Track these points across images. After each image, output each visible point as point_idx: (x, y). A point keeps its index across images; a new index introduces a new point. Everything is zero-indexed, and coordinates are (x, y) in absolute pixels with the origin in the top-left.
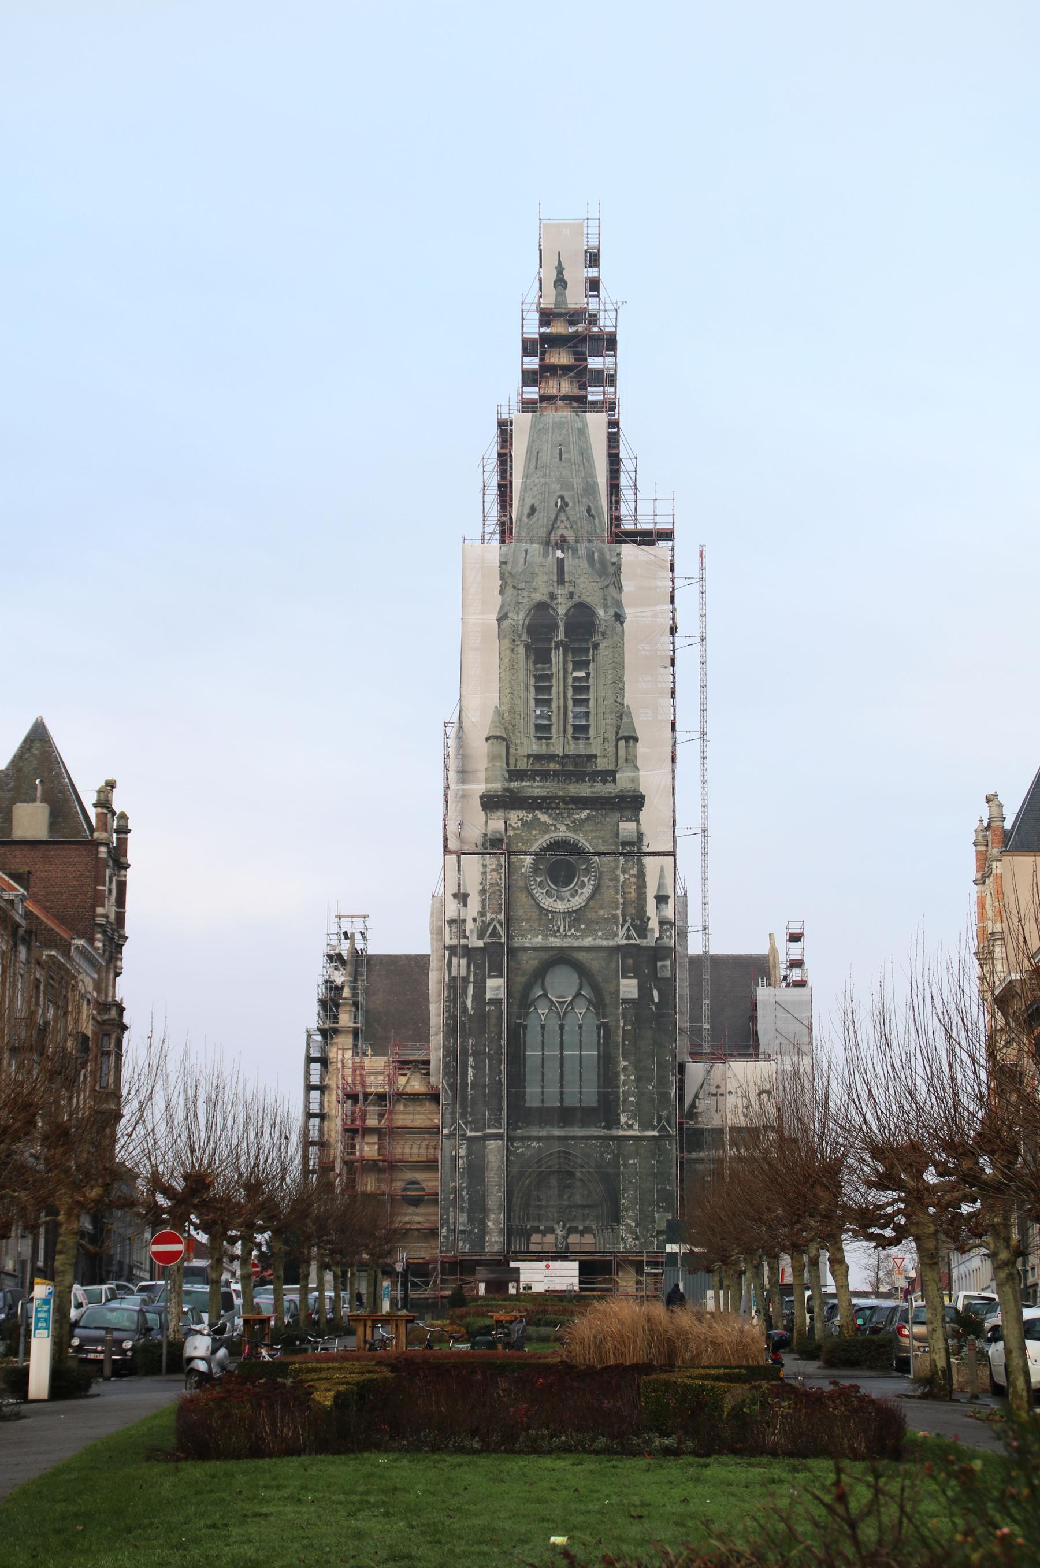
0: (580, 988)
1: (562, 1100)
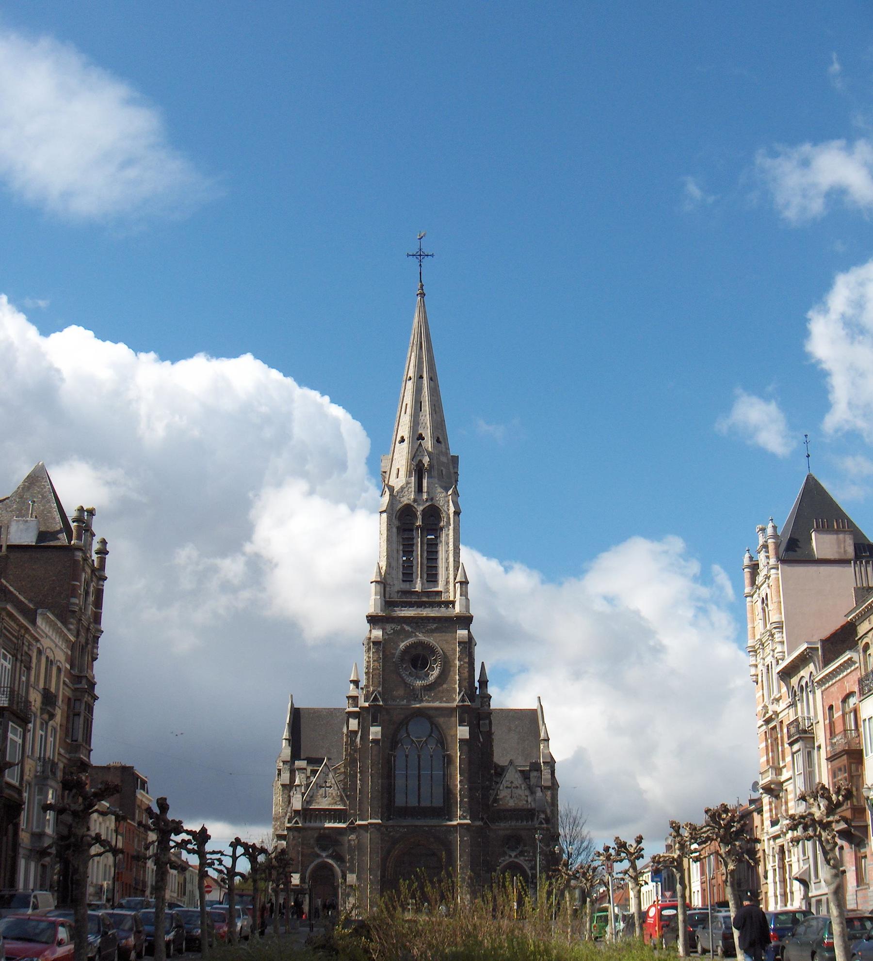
0: (432, 732)
1: (419, 802)
